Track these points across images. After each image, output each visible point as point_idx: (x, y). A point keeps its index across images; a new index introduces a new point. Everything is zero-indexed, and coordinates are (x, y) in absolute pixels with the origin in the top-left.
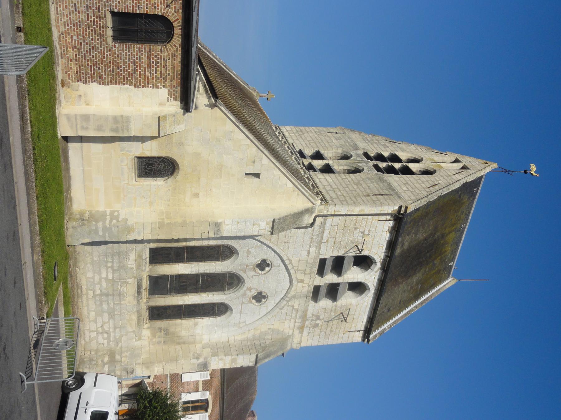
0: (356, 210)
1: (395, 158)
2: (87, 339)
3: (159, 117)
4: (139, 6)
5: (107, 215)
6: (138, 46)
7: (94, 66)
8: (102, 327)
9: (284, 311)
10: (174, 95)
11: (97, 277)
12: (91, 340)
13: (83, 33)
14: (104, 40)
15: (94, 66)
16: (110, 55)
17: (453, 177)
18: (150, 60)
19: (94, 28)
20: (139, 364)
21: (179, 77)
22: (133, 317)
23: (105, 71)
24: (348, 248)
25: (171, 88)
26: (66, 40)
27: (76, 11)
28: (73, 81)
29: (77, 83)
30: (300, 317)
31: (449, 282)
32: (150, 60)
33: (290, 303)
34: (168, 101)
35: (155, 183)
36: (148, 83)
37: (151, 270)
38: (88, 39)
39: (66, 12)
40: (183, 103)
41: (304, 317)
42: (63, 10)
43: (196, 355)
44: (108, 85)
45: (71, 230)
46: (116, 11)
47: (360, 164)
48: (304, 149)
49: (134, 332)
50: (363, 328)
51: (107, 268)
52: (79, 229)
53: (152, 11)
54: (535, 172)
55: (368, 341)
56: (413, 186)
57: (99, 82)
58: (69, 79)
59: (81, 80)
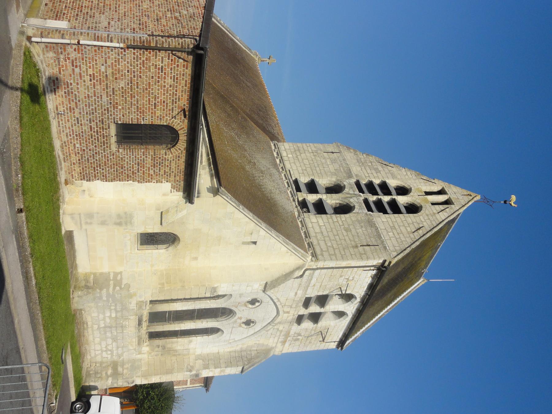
0: (344, 264)
1: (385, 188)
2: (93, 355)
3: (162, 213)
4: (143, 118)
5: (110, 280)
6: (143, 151)
7: (97, 167)
8: (106, 347)
9: (270, 332)
10: (177, 187)
11: (101, 316)
12: (96, 356)
13: (86, 142)
14: (107, 147)
15: (97, 167)
16: (113, 158)
17: (437, 215)
18: (154, 161)
19: (98, 137)
20: (139, 377)
21: (182, 173)
22: (134, 340)
23: (109, 171)
24: (332, 289)
25: (175, 182)
26: (69, 148)
27: (78, 123)
28: (76, 180)
29: (80, 181)
30: (283, 335)
31: (421, 282)
32: (154, 161)
33: (275, 327)
34: (171, 192)
35: (157, 251)
36: (152, 179)
37: (151, 308)
38: (92, 146)
39: (68, 125)
40: (186, 194)
41: (287, 335)
42: (66, 123)
43: (189, 367)
44: (112, 181)
45: (76, 299)
46: (119, 122)
47: (352, 200)
48: (300, 177)
49: (135, 349)
50: (338, 340)
51: (111, 310)
52: (84, 298)
53: (157, 122)
54: (514, 203)
55: (342, 349)
56: (399, 231)
57: (102, 180)
58: (73, 178)
59: (84, 179)
